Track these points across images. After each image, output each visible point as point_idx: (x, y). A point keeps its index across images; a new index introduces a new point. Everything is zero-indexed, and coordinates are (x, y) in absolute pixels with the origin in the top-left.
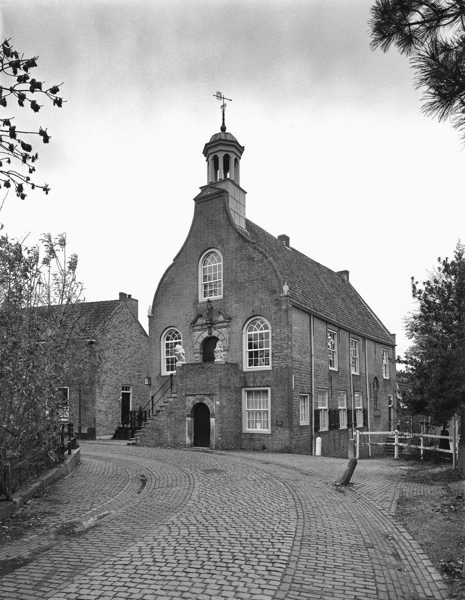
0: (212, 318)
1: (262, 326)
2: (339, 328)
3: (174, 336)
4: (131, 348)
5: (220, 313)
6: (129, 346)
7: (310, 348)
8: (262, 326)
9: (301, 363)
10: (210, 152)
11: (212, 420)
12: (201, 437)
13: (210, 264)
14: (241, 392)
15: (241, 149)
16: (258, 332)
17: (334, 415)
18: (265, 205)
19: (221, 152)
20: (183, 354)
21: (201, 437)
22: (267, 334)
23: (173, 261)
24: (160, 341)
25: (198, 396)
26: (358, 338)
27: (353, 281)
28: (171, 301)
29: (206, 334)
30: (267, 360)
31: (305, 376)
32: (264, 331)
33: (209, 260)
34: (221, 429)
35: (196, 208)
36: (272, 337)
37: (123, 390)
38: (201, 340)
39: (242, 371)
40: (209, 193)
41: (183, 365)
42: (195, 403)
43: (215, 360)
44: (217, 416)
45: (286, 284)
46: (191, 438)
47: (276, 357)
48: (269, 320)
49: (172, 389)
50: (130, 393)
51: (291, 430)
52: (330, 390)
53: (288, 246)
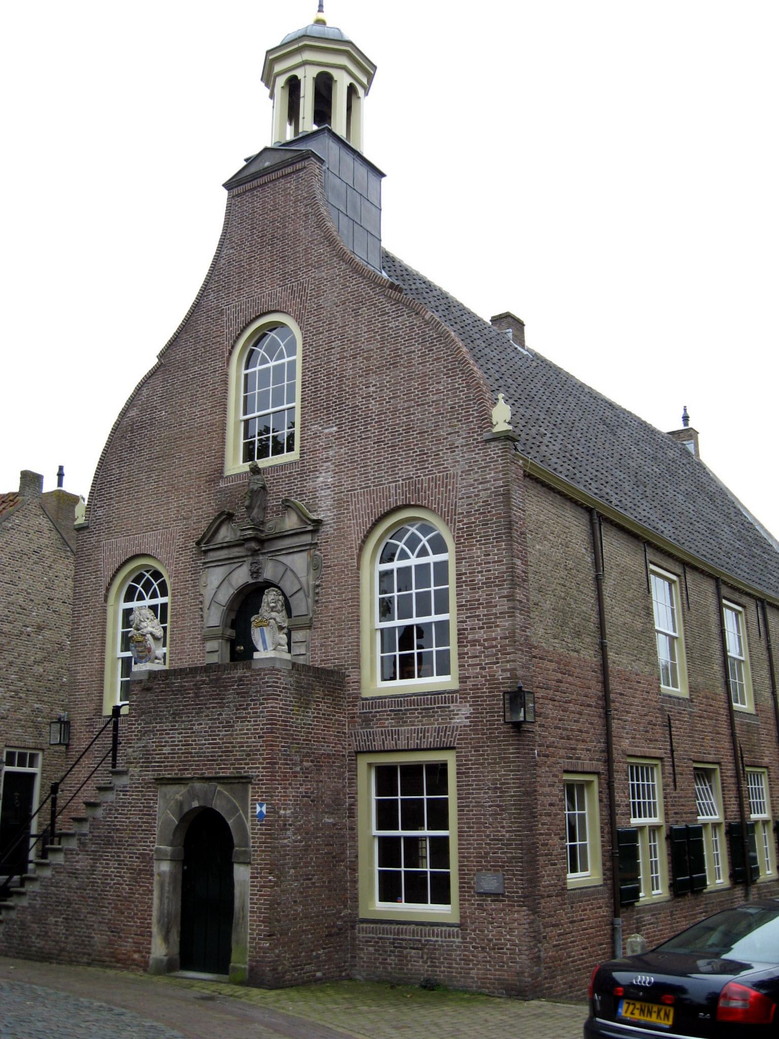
0: (263, 523)
1: (424, 540)
2: (685, 564)
3: (147, 586)
4: (47, 633)
5: (287, 505)
6: (40, 628)
7: (594, 617)
8: (424, 540)
9: (564, 667)
10: (278, 68)
11: (241, 873)
12: (204, 934)
13: (264, 361)
14: (354, 770)
15: (368, 69)
16: (413, 561)
17: (685, 847)
18: (446, 221)
19: (308, 67)
20: (156, 638)
21: (204, 934)
22: (441, 567)
23: (157, 360)
24: (106, 600)
25: (198, 785)
26: (744, 600)
27: (536, 340)
28: (143, 476)
29: (242, 576)
30: (444, 657)
31: (580, 713)
32: (432, 559)
33: (261, 351)
34: (273, 904)
35: (229, 207)
36: (459, 575)
37: (10, 762)
38: (225, 596)
39: (357, 697)
40: (267, 164)
41: (153, 675)
42: (186, 810)
43: (256, 655)
44: (258, 858)
45: (501, 401)
46: (166, 939)
47: (474, 642)
48: (442, 516)
49: (114, 758)
50: (33, 776)
51: (534, 911)
52: (668, 763)
53: (523, 346)
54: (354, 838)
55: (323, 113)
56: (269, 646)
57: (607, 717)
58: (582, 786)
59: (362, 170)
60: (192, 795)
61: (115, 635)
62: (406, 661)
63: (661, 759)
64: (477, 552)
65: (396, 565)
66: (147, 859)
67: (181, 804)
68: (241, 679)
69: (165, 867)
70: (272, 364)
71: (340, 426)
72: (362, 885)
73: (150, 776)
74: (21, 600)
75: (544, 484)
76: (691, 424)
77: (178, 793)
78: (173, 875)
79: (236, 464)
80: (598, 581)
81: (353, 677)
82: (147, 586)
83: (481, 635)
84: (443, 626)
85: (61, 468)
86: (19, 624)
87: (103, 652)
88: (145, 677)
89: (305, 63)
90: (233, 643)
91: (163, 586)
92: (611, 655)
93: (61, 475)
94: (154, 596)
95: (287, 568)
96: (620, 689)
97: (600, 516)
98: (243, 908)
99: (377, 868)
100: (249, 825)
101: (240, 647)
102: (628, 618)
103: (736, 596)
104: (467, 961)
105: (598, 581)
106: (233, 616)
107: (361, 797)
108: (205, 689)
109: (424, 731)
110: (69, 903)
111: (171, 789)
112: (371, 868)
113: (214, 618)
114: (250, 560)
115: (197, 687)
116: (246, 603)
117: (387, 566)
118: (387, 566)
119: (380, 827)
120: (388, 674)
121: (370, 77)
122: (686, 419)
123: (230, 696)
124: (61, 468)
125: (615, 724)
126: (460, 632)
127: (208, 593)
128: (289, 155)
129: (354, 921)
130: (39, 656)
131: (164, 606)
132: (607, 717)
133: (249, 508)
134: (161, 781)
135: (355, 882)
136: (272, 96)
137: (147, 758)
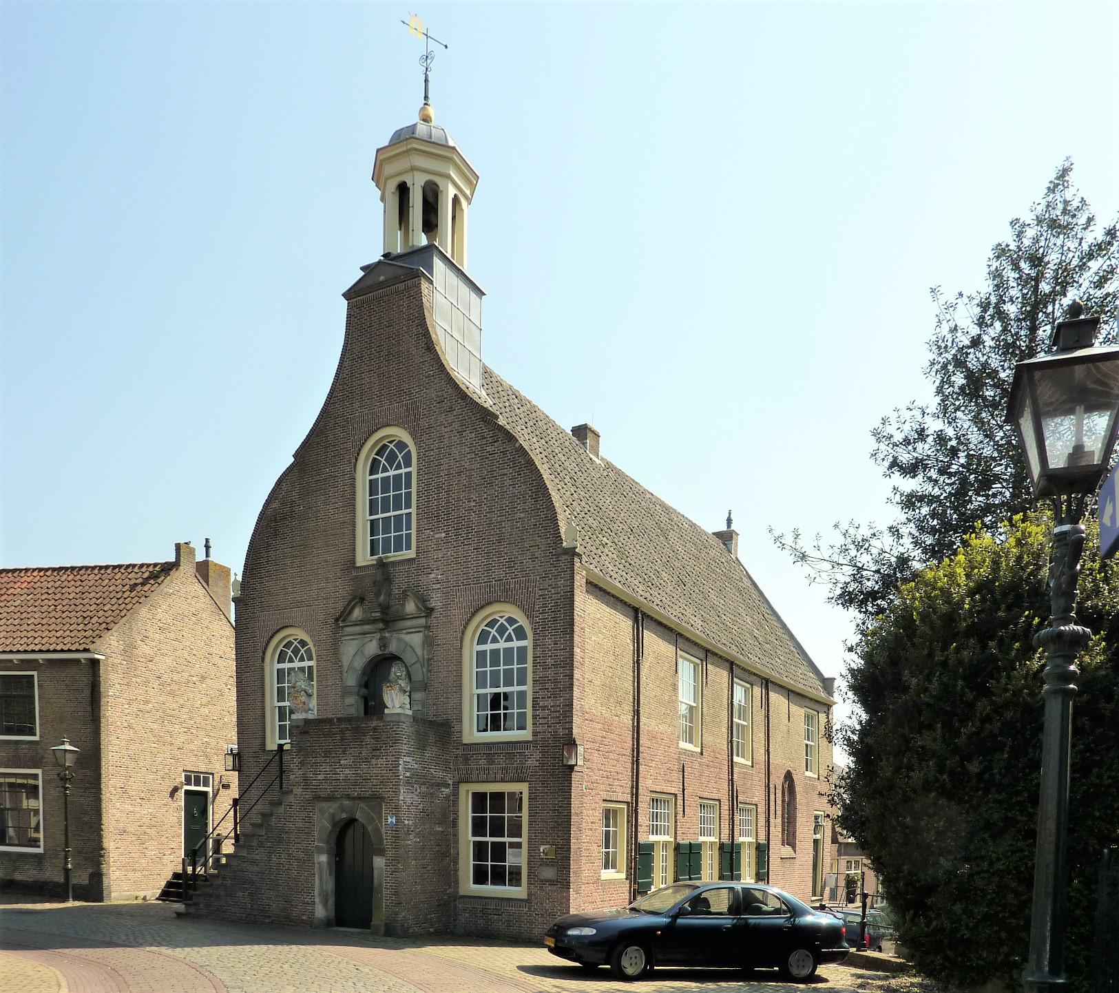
1: (510, 630)
3: (502, 630)
8: (510, 630)
9: (608, 727)
15: (471, 178)
16: (502, 645)
22: (522, 651)
25: (346, 802)
26: (753, 678)
27: (610, 450)
29: (372, 648)
30: (522, 716)
32: (516, 644)
38: (359, 663)
40: (382, 278)
43: (386, 711)
54: (457, 842)
55: (430, 225)
56: (396, 701)
57: (636, 762)
58: (615, 811)
59: (464, 289)
60: (342, 809)
61: (272, 689)
62: (495, 719)
63: (676, 795)
64: (548, 641)
65: (489, 647)
66: (309, 855)
67: (333, 815)
68: (375, 729)
69: (323, 858)
70: (391, 473)
71: (447, 532)
72: (461, 874)
73: (309, 796)
74: (186, 655)
75: (601, 589)
76: (733, 527)
77: (331, 808)
78: (329, 863)
79: (364, 557)
80: (637, 664)
81: (457, 728)
82: (296, 651)
83: (550, 703)
84: (522, 695)
85: (207, 540)
86: (186, 675)
87: (263, 702)
88: (301, 724)
89: (413, 169)
90: (366, 700)
91: (309, 652)
92: (642, 719)
93: (207, 547)
94: (302, 659)
95: (407, 645)
96: (648, 743)
97: (644, 614)
98: (380, 885)
99: (472, 862)
100: (383, 831)
101: (372, 704)
102: (658, 692)
103: (746, 676)
104: (531, 923)
105: (637, 664)
106: (366, 679)
107: (461, 813)
108: (348, 734)
109: (506, 769)
110: (252, 883)
111: (325, 805)
112: (467, 863)
113: (351, 681)
114: (378, 635)
115: (342, 732)
116: (376, 672)
117: (482, 648)
118: (482, 648)
119: (474, 835)
120: (482, 726)
121: (473, 187)
122: (729, 521)
123: (368, 739)
124: (207, 540)
125: (641, 768)
126: (535, 700)
127: (345, 661)
128: (401, 271)
129: (456, 897)
130: (204, 700)
131: (310, 668)
132: (636, 762)
133: (378, 595)
134: (317, 798)
135: (456, 871)
136: (383, 199)
137: (306, 782)
